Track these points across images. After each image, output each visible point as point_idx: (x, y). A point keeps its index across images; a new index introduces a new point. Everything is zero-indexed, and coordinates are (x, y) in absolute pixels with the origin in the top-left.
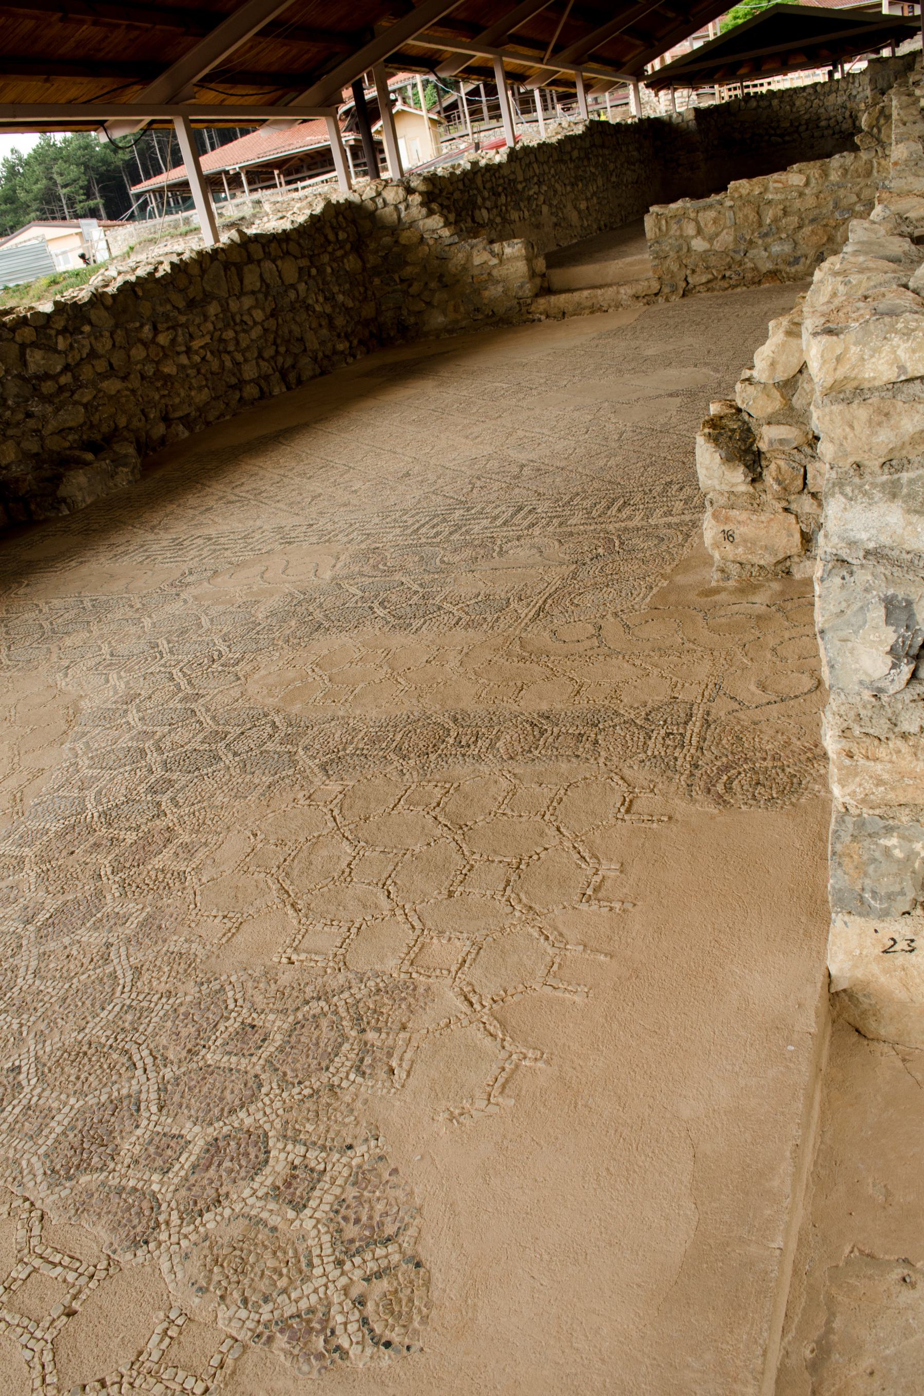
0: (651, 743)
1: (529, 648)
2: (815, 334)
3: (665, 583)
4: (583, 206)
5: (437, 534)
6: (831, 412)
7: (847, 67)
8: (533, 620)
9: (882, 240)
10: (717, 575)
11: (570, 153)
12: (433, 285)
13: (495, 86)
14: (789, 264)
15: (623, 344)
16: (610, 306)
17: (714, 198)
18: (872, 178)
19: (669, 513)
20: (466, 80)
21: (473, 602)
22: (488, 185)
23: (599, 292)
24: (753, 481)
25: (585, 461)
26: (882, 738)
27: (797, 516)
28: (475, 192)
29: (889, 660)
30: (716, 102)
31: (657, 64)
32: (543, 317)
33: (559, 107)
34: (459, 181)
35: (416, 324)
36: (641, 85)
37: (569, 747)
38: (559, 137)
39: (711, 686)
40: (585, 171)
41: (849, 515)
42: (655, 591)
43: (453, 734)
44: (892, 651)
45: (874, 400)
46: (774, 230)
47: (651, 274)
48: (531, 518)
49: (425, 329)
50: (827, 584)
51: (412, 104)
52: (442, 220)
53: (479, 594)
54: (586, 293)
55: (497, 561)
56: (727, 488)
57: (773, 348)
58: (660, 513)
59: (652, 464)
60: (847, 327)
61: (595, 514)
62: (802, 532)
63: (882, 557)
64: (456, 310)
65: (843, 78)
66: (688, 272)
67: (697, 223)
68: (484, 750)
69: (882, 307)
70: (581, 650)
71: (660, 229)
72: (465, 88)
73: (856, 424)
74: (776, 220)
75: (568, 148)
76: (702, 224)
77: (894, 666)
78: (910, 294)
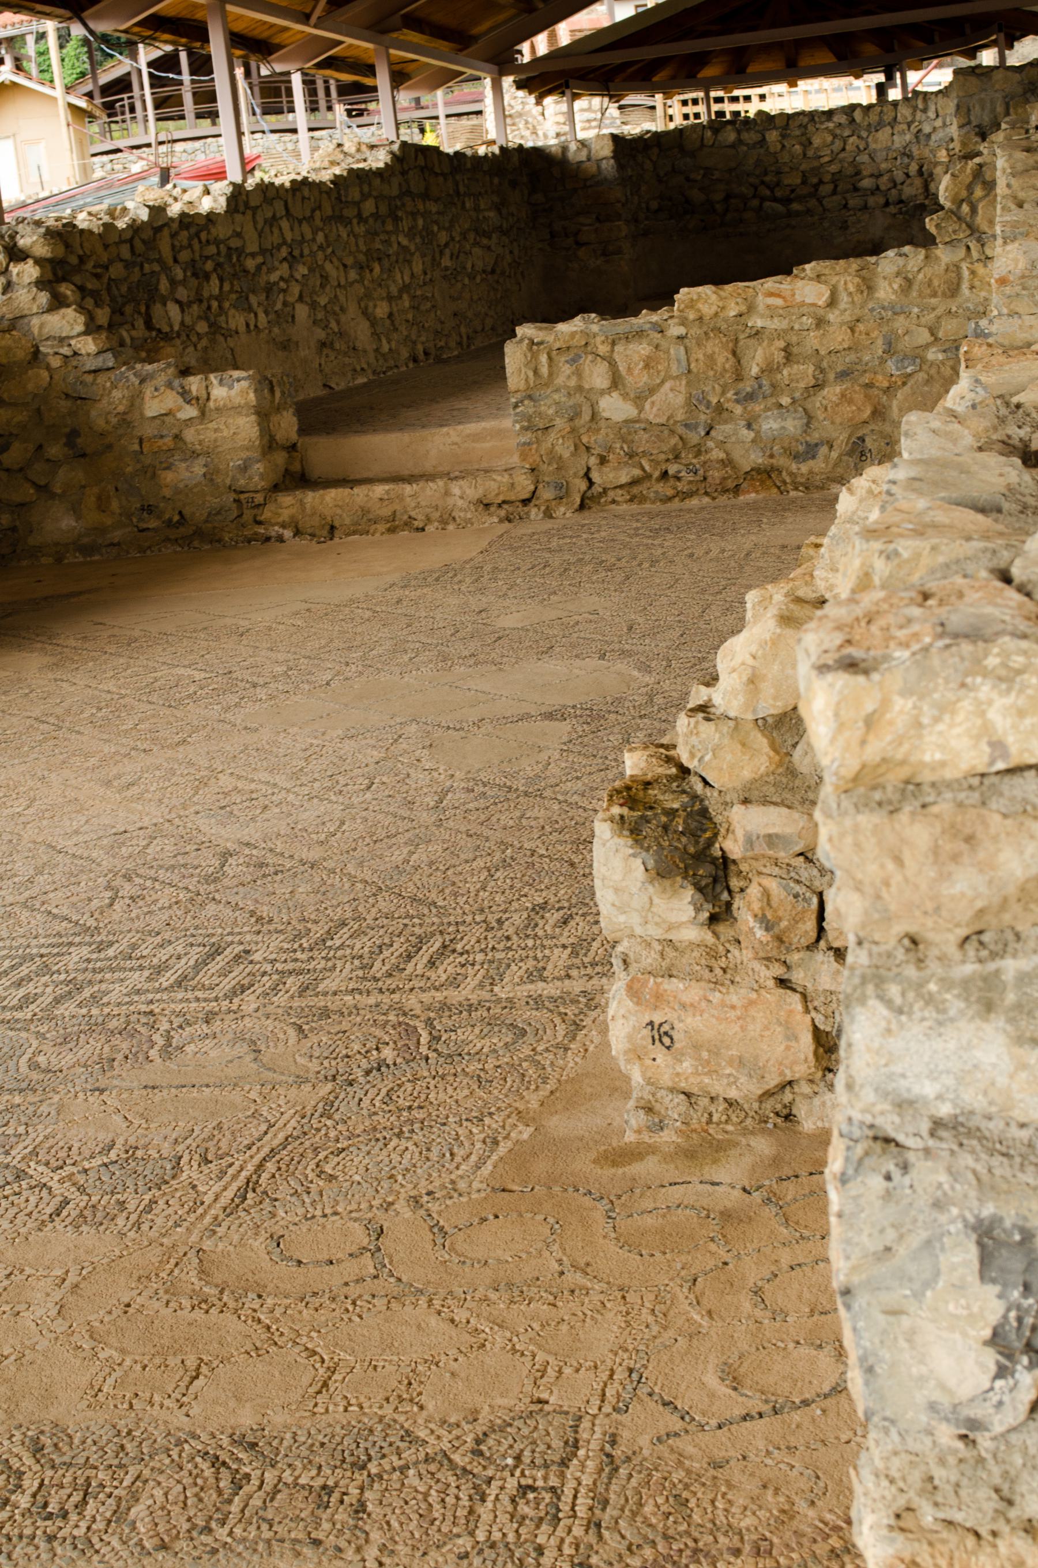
0: (484, 1511)
1: (218, 1278)
2: (822, 669)
3: (526, 1133)
4: (381, 310)
5: (27, 1000)
6: (856, 829)
7: (913, 77)
8: (229, 1211)
9: (966, 458)
10: (637, 1119)
11: (357, 204)
12: (55, 450)
13: (209, 58)
14: (796, 457)
15: (453, 601)
16: (429, 520)
17: (647, 318)
18: (959, 300)
19: (538, 974)
20: (146, 40)
21: (97, 1162)
22: (184, 256)
23: (408, 489)
24: (713, 919)
25: (362, 851)
26: (984, 1532)
27: (804, 996)
28: (157, 268)
29: (991, 1358)
30: (656, 125)
31: (542, 44)
32: (288, 534)
33: (340, 109)
34: (122, 242)
35: (14, 529)
36: (508, 81)
37: (298, 1519)
38: (337, 171)
39: (620, 1374)
40: (387, 242)
41: (895, 1044)
42: (503, 1149)
43: (30, 1484)
44: (996, 1339)
45: (944, 807)
46: (767, 388)
47: (515, 459)
48: (239, 974)
49: (33, 541)
50: (854, 1188)
51: (34, 71)
52: (81, 319)
53: (112, 1145)
54: (380, 490)
55: (157, 1069)
56: (656, 932)
57: (753, 648)
58: (516, 972)
59: (505, 864)
60: (887, 658)
61: (378, 969)
62: (816, 1031)
63: (969, 1134)
64: (102, 503)
65: (906, 99)
66: (593, 461)
67: (612, 364)
68: (100, 1525)
69: (957, 618)
70: (337, 1282)
71: (536, 372)
72: (146, 54)
73: (907, 856)
74: (770, 369)
75: (355, 194)
76: (622, 368)
77: (1002, 1372)
78: (1012, 595)
